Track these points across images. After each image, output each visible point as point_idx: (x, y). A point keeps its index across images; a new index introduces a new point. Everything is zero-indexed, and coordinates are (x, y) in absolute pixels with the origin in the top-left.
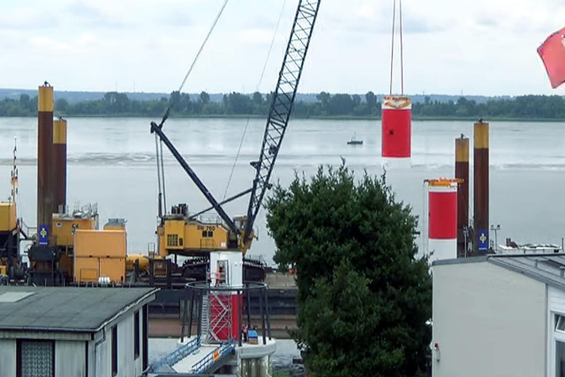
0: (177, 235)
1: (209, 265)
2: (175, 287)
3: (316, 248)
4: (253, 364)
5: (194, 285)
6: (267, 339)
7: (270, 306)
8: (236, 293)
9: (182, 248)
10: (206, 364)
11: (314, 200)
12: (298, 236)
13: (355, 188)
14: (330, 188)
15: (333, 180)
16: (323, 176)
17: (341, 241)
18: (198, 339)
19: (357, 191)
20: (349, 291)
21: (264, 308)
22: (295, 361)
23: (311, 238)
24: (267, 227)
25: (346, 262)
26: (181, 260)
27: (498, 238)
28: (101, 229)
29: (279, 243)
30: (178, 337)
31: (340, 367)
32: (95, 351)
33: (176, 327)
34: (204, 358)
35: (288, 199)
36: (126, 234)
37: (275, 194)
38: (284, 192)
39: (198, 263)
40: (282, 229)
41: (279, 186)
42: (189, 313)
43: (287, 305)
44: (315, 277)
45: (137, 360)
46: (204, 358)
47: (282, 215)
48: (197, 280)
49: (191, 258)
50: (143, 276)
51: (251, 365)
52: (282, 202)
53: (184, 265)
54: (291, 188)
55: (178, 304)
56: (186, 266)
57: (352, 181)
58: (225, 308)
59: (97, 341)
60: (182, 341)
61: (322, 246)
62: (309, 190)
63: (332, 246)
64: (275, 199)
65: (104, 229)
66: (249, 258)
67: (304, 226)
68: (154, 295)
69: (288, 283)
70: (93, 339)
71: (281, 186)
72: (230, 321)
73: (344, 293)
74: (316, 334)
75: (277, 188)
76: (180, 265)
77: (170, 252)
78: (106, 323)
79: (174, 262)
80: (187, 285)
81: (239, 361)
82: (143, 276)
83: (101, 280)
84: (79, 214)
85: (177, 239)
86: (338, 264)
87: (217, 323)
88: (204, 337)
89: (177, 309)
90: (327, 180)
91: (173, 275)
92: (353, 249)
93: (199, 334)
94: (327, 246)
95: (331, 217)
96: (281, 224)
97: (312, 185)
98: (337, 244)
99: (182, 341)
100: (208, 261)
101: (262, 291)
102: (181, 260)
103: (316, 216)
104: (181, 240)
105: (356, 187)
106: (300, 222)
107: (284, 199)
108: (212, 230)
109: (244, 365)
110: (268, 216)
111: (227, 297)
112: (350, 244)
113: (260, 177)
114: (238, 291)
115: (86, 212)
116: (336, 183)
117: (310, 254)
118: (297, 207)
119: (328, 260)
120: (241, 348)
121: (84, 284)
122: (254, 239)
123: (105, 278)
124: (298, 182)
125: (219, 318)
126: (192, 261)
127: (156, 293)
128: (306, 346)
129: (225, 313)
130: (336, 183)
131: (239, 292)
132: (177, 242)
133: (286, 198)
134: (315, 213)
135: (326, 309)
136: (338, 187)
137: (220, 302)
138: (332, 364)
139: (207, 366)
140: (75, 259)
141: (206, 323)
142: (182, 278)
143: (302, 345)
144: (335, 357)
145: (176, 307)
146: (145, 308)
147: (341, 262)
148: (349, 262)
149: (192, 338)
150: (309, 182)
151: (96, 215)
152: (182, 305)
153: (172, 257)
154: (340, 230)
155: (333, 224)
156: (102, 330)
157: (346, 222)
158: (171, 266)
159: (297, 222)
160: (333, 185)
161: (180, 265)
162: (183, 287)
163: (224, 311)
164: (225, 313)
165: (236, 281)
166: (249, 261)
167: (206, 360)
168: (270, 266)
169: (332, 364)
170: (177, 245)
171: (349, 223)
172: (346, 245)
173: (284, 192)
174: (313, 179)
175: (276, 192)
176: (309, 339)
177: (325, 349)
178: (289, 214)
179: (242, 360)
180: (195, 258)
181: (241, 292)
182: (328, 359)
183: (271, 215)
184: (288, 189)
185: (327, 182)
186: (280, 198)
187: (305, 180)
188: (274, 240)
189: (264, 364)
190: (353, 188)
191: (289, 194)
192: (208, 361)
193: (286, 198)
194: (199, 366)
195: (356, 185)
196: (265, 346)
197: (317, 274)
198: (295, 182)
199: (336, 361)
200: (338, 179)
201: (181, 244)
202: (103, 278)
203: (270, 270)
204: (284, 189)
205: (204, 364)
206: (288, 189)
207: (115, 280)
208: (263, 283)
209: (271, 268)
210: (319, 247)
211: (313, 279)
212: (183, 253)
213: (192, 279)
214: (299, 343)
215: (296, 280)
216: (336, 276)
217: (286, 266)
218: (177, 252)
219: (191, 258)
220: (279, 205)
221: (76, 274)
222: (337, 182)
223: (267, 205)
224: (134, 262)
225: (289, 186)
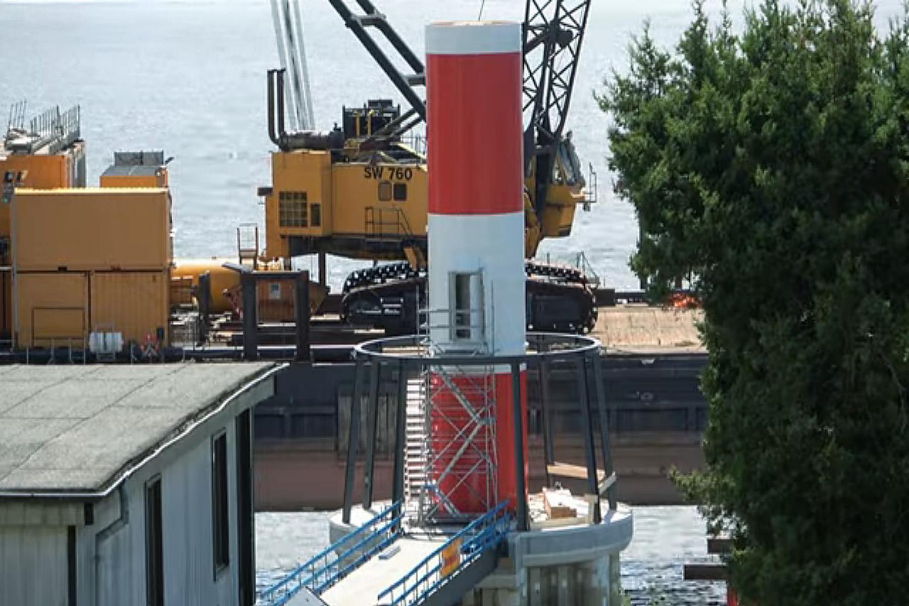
0: (304, 196)
1: (423, 285)
2: (322, 356)
3: (760, 228)
4: (564, 584)
5: (378, 347)
6: (605, 506)
7: (614, 406)
8: (507, 369)
9: (317, 232)
10: (421, 588)
11: (755, 82)
12: (704, 193)
13: (878, 43)
14: (802, 47)
15: (811, 19)
16: (780, 9)
17: (842, 206)
18: (396, 512)
19: (885, 51)
20: (865, 358)
21: (593, 413)
22: (692, 573)
23: (745, 199)
24: (611, 168)
25: (853, 271)
26: (340, 271)
27: (30, 325)
28: (93, 187)
29: (650, 215)
30: (332, 508)
31: (838, 587)
32: (97, 558)
33: (328, 474)
34: (416, 570)
35: (674, 82)
36: (170, 197)
37: (636, 66)
38: (663, 60)
39: (389, 281)
40: (658, 174)
41: (648, 45)
42: (364, 435)
43: (664, 404)
44: (756, 315)
45: (222, 581)
46: (416, 570)
47: (656, 130)
48: (387, 335)
49: (368, 264)
50: (223, 327)
51: (556, 588)
52: (655, 91)
53: (346, 288)
54: (683, 47)
55: (332, 410)
56: (353, 291)
57: (868, 23)
58: (475, 418)
59: (102, 528)
60: (346, 519)
61: (777, 224)
62: (740, 54)
63: (806, 223)
64: (633, 79)
65: (102, 185)
66: (545, 264)
67: (722, 164)
68: (271, 381)
69: (674, 331)
70: (89, 520)
71: (653, 44)
72: (492, 455)
73: (847, 363)
74: (764, 487)
75: (641, 49)
76: (336, 286)
77: (301, 246)
78: (128, 473)
79: (315, 279)
80: (358, 347)
81: (521, 576)
82: (223, 327)
83: (96, 341)
84: (23, 140)
85: (305, 205)
86: (830, 275)
87: (452, 464)
88: (411, 507)
89: (327, 424)
90: (792, 21)
91: (313, 318)
92: (872, 231)
93: (397, 495)
94: (794, 224)
95: (804, 134)
96: (652, 159)
97: (745, 38)
98: (825, 216)
99: (346, 519)
100: (422, 275)
101: (592, 360)
102: (340, 271)
103: (759, 131)
104: (315, 207)
105: (883, 42)
106: (711, 151)
107: (661, 83)
108: (404, 181)
109: (537, 587)
110: (614, 136)
111: (479, 381)
112: (864, 216)
113: (562, 13)
114: (514, 361)
115: (45, 134)
116: (819, 29)
117: (741, 249)
118: (702, 104)
119: (800, 262)
120: (524, 535)
121: (43, 353)
122: (579, 206)
123: (109, 335)
124: (703, 29)
125: (458, 445)
126: (373, 273)
127: (275, 376)
128: (733, 527)
129: (475, 431)
130: (819, 29)
131: (516, 368)
132: (304, 214)
133: (668, 79)
134: (757, 121)
135: (793, 411)
136: (833, 39)
137: (461, 399)
138: (816, 579)
139: (425, 594)
140: (16, 279)
141: (417, 464)
142: (345, 330)
143: (721, 522)
144: (825, 559)
145: (330, 415)
146: (243, 420)
147: (839, 270)
148: (862, 270)
149: (379, 507)
150: (739, 30)
151: (75, 140)
152: (345, 406)
153: (305, 263)
154: (834, 173)
155: (811, 152)
156: (117, 494)
157: (852, 148)
158: (308, 292)
159: (701, 151)
160: (809, 36)
161: (336, 286)
162: (345, 356)
163: (475, 424)
164: (475, 431)
165: (508, 331)
166: (546, 271)
167: (422, 573)
168: (608, 286)
169: (816, 579)
170: (304, 225)
171: (860, 151)
172: (851, 217)
173: (663, 60)
174: (751, 19)
175: (640, 60)
176: (745, 505)
177: (791, 536)
178: (676, 127)
179: (529, 570)
180: (381, 264)
181: (523, 367)
182: (801, 563)
183: (622, 130)
184: (673, 53)
185: (791, 28)
186: (650, 78)
187: (726, 23)
188: (632, 207)
189: (595, 583)
190: (873, 44)
191: (678, 68)
192: (425, 578)
193: (668, 79)
194: (398, 592)
195: (882, 32)
196: (596, 527)
197: (763, 308)
198: (693, 29)
199: (826, 569)
200: (826, 18)
201: (316, 222)
202: (101, 335)
203: (609, 298)
204: (661, 52)
205: (415, 587)
206: (673, 53)
207: (140, 340)
208: (588, 337)
209: (613, 291)
210: (769, 225)
211: (753, 323)
212: (350, 247)
213: (373, 331)
214: (713, 519)
215: (700, 328)
216: (825, 314)
217: (666, 284)
218: (322, 246)
219: (368, 264)
220: (648, 99)
221: (19, 322)
222: (823, 26)
223: (611, 98)
224: (195, 283)
225: (678, 44)
